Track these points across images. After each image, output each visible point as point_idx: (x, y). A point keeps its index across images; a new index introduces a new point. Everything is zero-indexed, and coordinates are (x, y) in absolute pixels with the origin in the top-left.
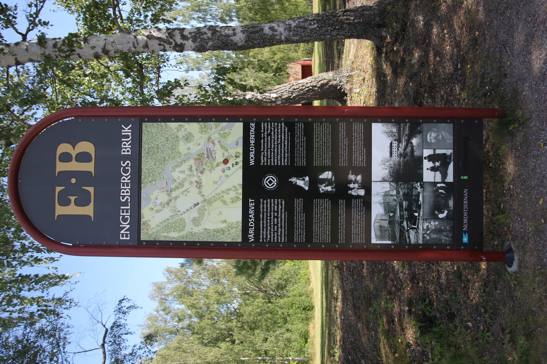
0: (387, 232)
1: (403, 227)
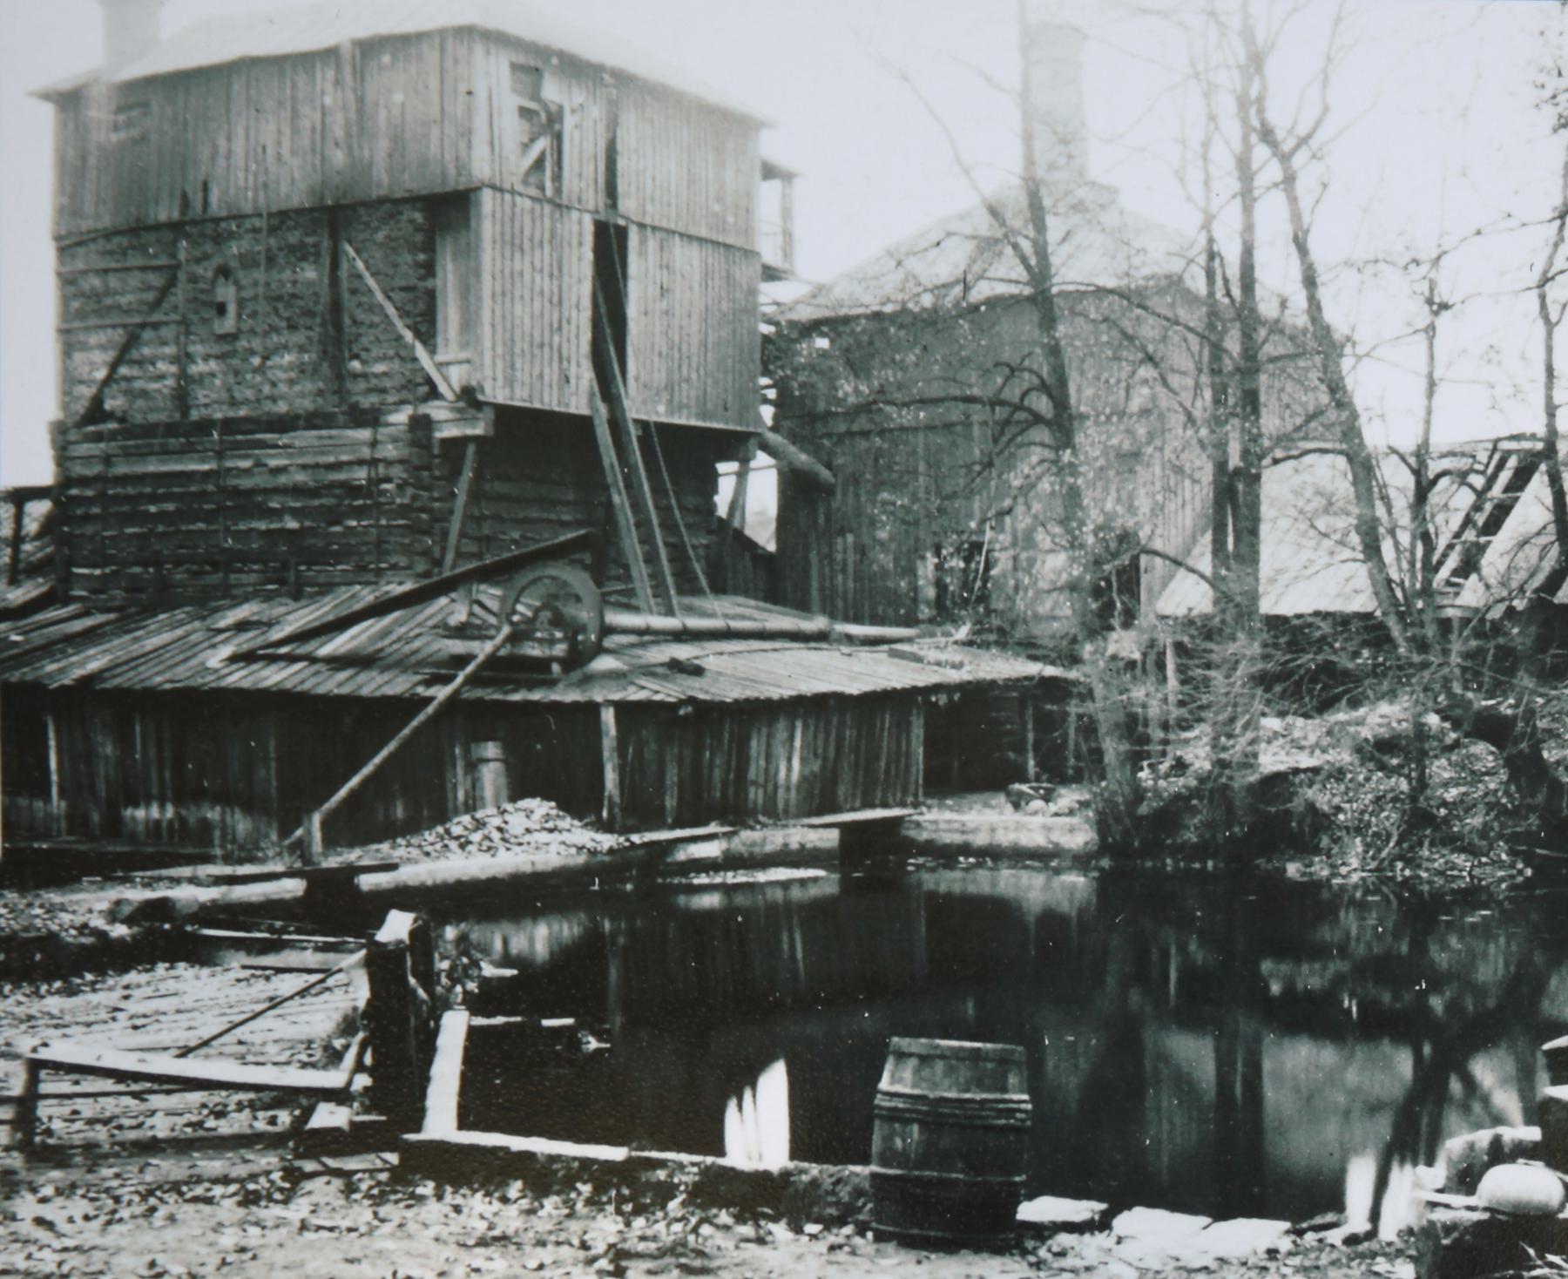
0: (285, 376)
1: (424, 801)
